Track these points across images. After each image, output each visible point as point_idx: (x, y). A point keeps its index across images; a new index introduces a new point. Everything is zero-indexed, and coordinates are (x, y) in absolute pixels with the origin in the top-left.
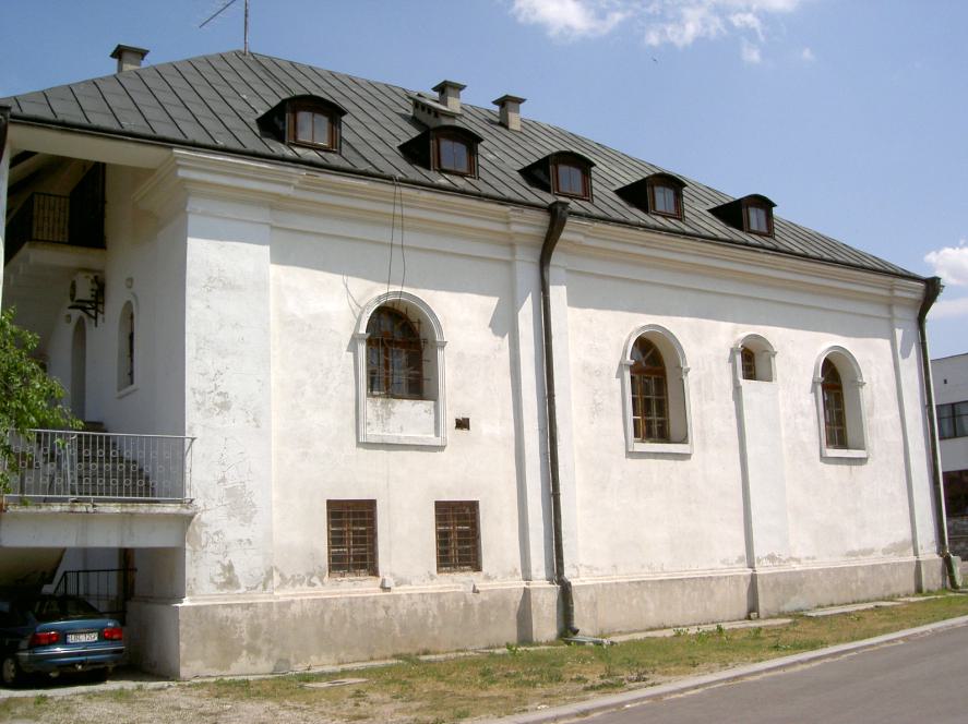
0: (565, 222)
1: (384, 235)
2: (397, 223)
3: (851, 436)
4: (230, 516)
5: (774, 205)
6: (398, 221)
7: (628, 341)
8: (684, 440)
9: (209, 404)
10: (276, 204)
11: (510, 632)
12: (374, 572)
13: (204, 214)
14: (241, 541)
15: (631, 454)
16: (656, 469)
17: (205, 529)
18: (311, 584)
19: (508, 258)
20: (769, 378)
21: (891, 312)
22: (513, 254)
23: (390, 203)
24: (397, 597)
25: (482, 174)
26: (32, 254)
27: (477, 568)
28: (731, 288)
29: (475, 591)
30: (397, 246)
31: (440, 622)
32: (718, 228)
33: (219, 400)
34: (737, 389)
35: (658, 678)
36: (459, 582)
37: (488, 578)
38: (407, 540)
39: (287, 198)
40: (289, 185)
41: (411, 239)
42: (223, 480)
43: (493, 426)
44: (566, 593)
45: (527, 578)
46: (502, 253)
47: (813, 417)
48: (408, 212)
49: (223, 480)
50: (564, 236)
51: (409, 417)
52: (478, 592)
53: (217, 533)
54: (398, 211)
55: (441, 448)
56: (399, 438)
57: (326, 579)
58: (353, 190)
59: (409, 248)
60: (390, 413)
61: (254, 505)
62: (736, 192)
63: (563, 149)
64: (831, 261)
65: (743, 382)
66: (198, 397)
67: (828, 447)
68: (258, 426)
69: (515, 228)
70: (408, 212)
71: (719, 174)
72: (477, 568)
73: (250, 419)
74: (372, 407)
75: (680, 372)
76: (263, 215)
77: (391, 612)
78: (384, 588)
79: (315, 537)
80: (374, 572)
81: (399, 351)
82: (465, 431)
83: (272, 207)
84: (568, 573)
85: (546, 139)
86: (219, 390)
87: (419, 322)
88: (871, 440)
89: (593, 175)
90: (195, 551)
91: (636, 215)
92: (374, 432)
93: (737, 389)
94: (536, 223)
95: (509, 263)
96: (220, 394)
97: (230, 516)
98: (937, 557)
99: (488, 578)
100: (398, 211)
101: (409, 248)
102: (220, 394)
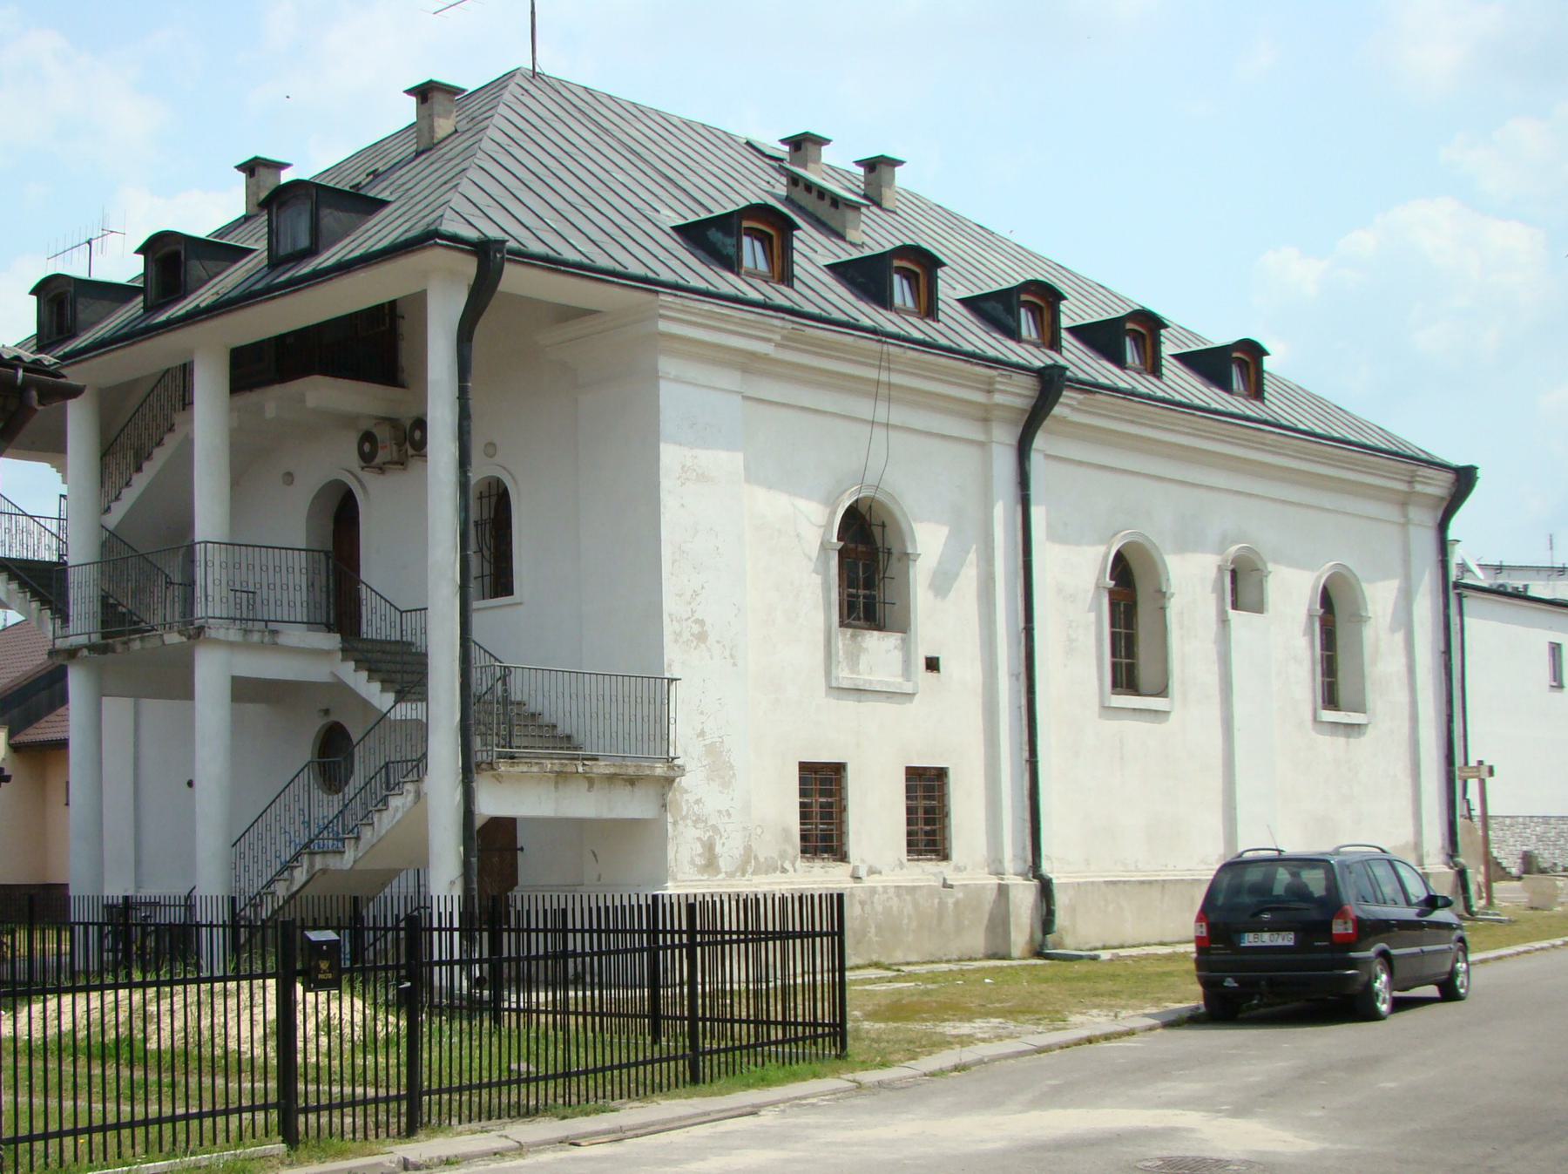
0: (1059, 395)
1: (864, 408)
2: (878, 391)
3: (1145, 673)
4: (709, 779)
5: (1264, 353)
6: (883, 391)
7: (1107, 554)
8: (1162, 692)
9: (686, 635)
10: (749, 364)
11: (976, 940)
12: (841, 856)
13: (677, 380)
14: (720, 812)
15: (1107, 710)
16: (1134, 732)
17: (686, 796)
18: (784, 871)
19: (981, 437)
20: (1258, 607)
21: (1405, 516)
22: (988, 432)
23: (872, 366)
24: (873, 891)
25: (941, 316)
26: (414, 413)
27: (945, 856)
28: (1220, 479)
29: (945, 885)
30: (880, 424)
31: (914, 924)
32: (842, 301)
33: (696, 629)
34: (1224, 621)
35: (1075, 1019)
36: (926, 872)
37: (958, 869)
38: (875, 814)
39: (765, 358)
40: (769, 340)
41: (899, 415)
42: (702, 734)
43: (963, 668)
44: (1046, 890)
45: (999, 873)
46: (972, 431)
47: (1307, 665)
48: (896, 379)
49: (702, 734)
50: (1057, 410)
51: (878, 646)
52: (951, 887)
53: (698, 802)
54: (884, 376)
55: (910, 696)
56: (871, 682)
57: (799, 862)
58: (724, 318)
59: (895, 427)
60: (861, 649)
61: (732, 767)
62: (1220, 335)
63: (908, 242)
64: (546, 259)
65: (1232, 613)
66: (676, 626)
67: (1325, 708)
68: (735, 665)
69: (998, 398)
70: (896, 379)
71: (1201, 321)
72: (945, 856)
73: (727, 653)
74: (842, 638)
75: (1161, 595)
76: (729, 379)
77: (868, 908)
78: (856, 878)
79: (782, 807)
80: (841, 856)
81: (867, 569)
82: (935, 674)
83: (745, 370)
84: (1046, 868)
85: (584, 133)
86: (697, 616)
87: (883, 526)
88: (1372, 698)
89: (796, 244)
90: (675, 823)
91: (868, 314)
92: (844, 675)
93: (1224, 621)
94: (1016, 394)
95: (982, 445)
96: (697, 621)
97: (709, 779)
98: (1447, 869)
99: (958, 869)
100: (884, 376)
101: (895, 427)
102: (697, 621)
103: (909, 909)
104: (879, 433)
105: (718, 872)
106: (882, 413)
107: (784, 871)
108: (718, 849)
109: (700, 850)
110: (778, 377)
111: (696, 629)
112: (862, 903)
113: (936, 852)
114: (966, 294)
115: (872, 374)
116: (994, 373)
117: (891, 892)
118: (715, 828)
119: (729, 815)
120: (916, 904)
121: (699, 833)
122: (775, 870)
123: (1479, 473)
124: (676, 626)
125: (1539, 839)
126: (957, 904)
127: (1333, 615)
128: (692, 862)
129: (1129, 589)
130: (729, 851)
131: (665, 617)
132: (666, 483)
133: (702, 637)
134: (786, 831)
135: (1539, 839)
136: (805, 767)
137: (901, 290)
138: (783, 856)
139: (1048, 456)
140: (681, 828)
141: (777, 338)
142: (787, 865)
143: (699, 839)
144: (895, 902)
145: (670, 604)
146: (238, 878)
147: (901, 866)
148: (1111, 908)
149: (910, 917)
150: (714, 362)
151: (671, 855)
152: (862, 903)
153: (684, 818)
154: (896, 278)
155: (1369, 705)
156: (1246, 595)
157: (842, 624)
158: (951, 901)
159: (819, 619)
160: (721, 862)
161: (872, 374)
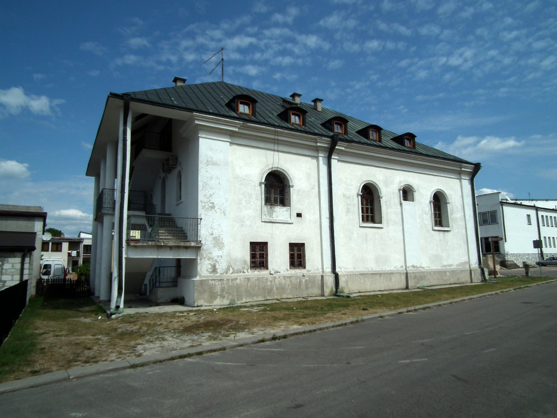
0: (337, 143)
9: (207, 207)
10: (231, 134)
18: (244, 272)
19: (316, 155)
25: (307, 125)
31: (290, 287)
33: (211, 205)
34: (401, 204)
42: (212, 234)
43: (311, 216)
46: (315, 154)
48: (280, 138)
49: (212, 234)
54: (276, 137)
60: (273, 211)
61: (223, 243)
70: (280, 138)
73: (222, 212)
75: (379, 198)
77: (273, 283)
82: (300, 218)
84: (338, 270)
90: (201, 259)
91: (364, 140)
92: (267, 218)
96: (211, 203)
99: (308, 271)
100: (276, 137)
102: (211, 203)
103: (288, 282)
104: (276, 153)
105: (217, 273)
106: (276, 148)
107: (244, 272)
108: (217, 266)
109: (210, 267)
110: (286, 145)
111: (211, 205)
112: (271, 281)
113: (263, 266)
114: (392, 137)
115: (273, 137)
116: (316, 137)
117: (282, 278)
118: (216, 261)
119: (222, 257)
120: (291, 281)
121: (209, 262)
122: (240, 272)
123: (481, 165)
124: (203, 204)
125: (527, 259)
126: (306, 281)
127: (439, 201)
128: (207, 270)
129: (369, 195)
130: (221, 267)
131: (199, 201)
132: (201, 165)
133: (213, 207)
134: (245, 262)
135: (527, 259)
136: (252, 244)
137: (407, 143)
138: (244, 268)
139: (339, 161)
140: (203, 260)
141: (239, 126)
142: (245, 271)
143: (210, 264)
144: (283, 281)
145: (201, 197)
146: (344, 275)
147: (288, 270)
148: (362, 281)
149: (288, 285)
150: (271, 142)
151: (199, 268)
152: (271, 281)
153: (205, 258)
154: (406, 140)
155: (450, 225)
156: (409, 196)
157: (265, 204)
158: (304, 280)
159: (259, 203)
160: (218, 270)
161: (273, 137)
